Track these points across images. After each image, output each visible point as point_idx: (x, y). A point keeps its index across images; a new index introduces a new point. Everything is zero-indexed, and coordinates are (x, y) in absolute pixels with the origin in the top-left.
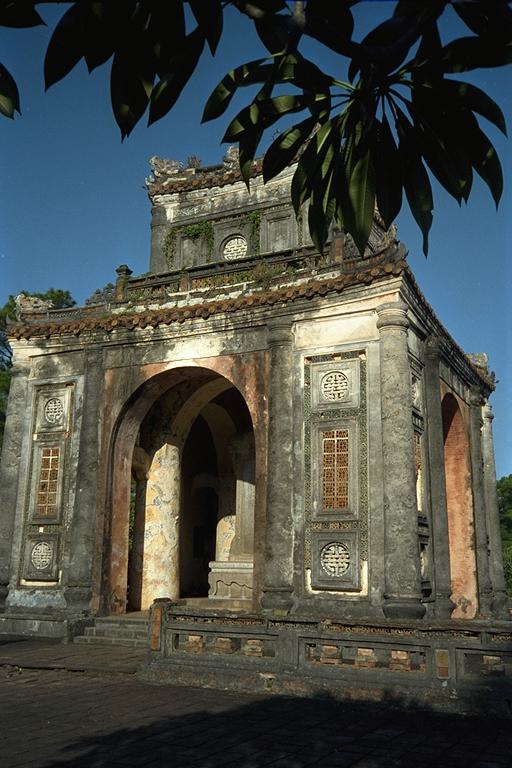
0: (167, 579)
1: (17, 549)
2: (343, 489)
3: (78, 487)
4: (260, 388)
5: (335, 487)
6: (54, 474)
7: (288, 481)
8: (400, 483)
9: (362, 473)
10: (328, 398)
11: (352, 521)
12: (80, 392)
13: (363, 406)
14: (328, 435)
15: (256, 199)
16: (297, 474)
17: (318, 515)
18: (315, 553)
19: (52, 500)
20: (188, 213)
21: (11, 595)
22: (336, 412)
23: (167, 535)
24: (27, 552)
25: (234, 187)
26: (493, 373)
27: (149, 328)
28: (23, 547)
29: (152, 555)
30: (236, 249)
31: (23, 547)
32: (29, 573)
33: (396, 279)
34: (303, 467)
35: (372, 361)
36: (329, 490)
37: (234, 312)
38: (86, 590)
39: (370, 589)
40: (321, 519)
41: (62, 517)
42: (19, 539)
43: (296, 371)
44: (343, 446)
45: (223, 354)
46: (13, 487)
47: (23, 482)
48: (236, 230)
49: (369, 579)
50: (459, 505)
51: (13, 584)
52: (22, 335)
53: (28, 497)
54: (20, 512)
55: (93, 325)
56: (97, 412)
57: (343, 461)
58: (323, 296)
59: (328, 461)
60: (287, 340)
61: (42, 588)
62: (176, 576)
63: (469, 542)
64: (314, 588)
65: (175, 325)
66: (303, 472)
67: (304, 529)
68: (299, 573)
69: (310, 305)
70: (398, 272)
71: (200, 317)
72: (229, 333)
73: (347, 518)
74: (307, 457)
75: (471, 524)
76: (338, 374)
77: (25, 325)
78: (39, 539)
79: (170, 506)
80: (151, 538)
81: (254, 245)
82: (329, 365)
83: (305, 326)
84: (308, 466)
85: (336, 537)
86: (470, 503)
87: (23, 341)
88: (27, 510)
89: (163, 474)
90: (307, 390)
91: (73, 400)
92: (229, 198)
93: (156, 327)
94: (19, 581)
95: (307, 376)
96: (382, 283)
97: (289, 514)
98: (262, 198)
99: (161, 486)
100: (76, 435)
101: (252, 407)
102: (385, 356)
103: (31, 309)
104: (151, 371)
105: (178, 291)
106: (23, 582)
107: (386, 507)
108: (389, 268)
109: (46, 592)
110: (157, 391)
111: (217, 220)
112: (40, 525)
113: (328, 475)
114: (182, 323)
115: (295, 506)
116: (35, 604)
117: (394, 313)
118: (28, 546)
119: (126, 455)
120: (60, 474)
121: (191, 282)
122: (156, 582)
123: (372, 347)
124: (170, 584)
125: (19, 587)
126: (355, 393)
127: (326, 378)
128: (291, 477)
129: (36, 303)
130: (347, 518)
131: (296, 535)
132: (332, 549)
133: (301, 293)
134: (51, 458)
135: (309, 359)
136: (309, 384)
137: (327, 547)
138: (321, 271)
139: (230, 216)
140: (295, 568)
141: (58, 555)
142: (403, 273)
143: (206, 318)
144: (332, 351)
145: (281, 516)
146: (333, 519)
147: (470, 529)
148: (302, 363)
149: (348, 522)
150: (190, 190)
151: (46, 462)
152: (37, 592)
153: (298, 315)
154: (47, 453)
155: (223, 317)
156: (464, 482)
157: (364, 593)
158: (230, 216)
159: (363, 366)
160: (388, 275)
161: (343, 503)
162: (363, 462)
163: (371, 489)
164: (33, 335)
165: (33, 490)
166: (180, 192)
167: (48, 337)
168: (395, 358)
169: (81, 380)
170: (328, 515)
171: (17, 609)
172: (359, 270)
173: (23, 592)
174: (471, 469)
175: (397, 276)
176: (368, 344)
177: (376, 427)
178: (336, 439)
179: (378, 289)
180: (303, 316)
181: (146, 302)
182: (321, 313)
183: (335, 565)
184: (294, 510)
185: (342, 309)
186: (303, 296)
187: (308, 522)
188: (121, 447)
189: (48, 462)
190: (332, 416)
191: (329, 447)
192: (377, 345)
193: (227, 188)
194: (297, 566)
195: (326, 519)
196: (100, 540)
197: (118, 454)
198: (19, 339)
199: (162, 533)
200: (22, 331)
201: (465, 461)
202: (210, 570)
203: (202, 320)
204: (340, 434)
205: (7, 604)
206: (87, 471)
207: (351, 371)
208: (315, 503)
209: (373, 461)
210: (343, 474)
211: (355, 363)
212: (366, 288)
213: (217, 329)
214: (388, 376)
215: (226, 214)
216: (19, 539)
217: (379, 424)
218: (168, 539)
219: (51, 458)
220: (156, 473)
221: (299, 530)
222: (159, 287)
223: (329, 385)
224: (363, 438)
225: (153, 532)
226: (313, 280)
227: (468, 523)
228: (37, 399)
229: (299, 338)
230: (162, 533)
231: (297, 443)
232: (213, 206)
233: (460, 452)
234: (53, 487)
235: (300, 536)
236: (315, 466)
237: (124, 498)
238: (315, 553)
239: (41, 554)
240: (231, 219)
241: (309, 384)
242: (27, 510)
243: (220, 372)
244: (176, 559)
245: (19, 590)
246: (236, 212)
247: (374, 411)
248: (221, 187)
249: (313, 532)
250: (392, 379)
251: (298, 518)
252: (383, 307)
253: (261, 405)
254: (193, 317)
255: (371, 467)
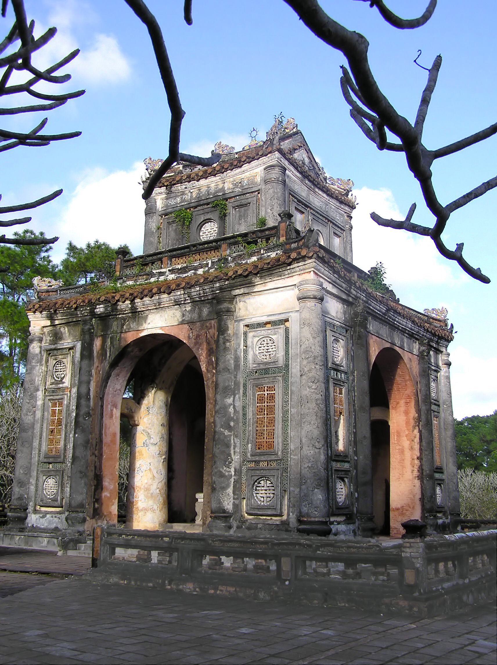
0: (155, 507)
1: (33, 481)
2: (272, 434)
3: (75, 433)
4: (210, 352)
5: (265, 433)
6: (60, 423)
7: (230, 428)
8: (311, 428)
9: (285, 421)
10: (261, 358)
11: (277, 460)
12: (78, 355)
13: (287, 366)
14: (262, 389)
15: (224, 191)
16: (236, 421)
17: (252, 455)
18: (249, 485)
19: (58, 442)
20: (172, 202)
21: (29, 519)
22: (266, 371)
23: (155, 472)
24: (40, 484)
25: (207, 180)
26: (452, 325)
27: (128, 302)
28: (37, 480)
29: (142, 487)
30: (209, 231)
31: (37, 480)
32: (42, 501)
33: (310, 261)
34: (241, 414)
35: (294, 326)
36: (259, 434)
37: (190, 288)
38: (81, 515)
39: (288, 515)
40: (254, 459)
41: (65, 456)
42: (34, 474)
43: (236, 334)
44: (272, 397)
45: (182, 323)
46: (30, 433)
47: (37, 426)
48: (208, 216)
49: (289, 507)
50: (408, 442)
51: (30, 509)
52: (36, 310)
53: (40, 441)
54: (35, 452)
55: (87, 301)
56: (90, 371)
57: (271, 410)
58: (256, 274)
59: (261, 410)
60: (229, 312)
61: (51, 512)
62: (164, 504)
63: (416, 473)
64: (249, 514)
65: (147, 300)
66: (241, 420)
67: (241, 467)
68: (237, 502)
69: (247, 282)
70: (310, 255)
71: (164, 292)
72: (187, 305)
73: (273, 457)
74: (244, 408)
75: (418, 458)
76: (269, 339)
77: (39, 302)
78: (49, 474)
79: (157, 448)
80: (141, 474)
81: (222, 228)
82: (262, 332)
83: (247, 299)
84: (244, 415)
85: (264, 473)
86: (417, 440)
87: (38, 314)
88: (40, 451)
89: (152, 416)
90: (246, 352)
91: (73, 363)
92: (204, 190)
93: (132, 301)
94: (35, 507)
95: (245, 341)
96: (300, 264)
97: (230, 455)
98: (229, 189)
99: (149, 431)
100: (74, 390)
101: (203, 368)
102: (303, 323)
103: (46, 288)
104: (130, 337)
105: (161, 268)
106: (38, 508)
107: (301, 448)
108: (304, 252)
109: (54, 516)
110: (136, 352)
111: (196, 207)
112: (50, 463)
113: (259, 422)
114: (151, 297)
115: (234, 449)
116: (46, 524)
117: (309, 288)
118: (41, 480)
119: (115, 406)
120: (64, 423)
121: (171, 261)
122: (145, 510)
123: (294, 317)
124: (158, 512)
125: (35, 511)
126: (281, 354)
127: (260, 342)
128: (232, 424)
129: (49, 282)
130: (273, 457)
131: (235, 472)
132: (262, 482)
133: (239, 273)
134: (57, 408)
135: (247, 326)
136: (246, 347)
137: (258, 481)
138: (268, 250)
139: (204, 204)
140: (234, 499)
141: (62, 487)
142: (315, 256)
143: (169, 294)
144: (265, 319)
145: (222, 457)
146: (262, 458)
147: (417, 462)
148: (242, 329)
149: (274, 460)
150: (175, 184)
151: (54, 412)
152: (48, 516)
153: (237, 291)
154: (54, 405)
155: (182, 292)
156: (412, 422)
157: (285, 518)
158: (204, 204)
159: (287, 330)
160: (303, 258)
161: (271, 445)
162: (285, 413)
163: (292, 433)
164: (44, 309)
165: (44, 434)
166: (166, 186)
167: (55, 311)
168: (309, 325)
169: (79, 345)
170: (260, 455)
171: (34, 529)
172: (292, 250)
173: (37, 516)
174: (418, 411)
175: (310, 258)
176: (291, 314)
177: (296, 382)
178: (266, 393)
179: (297, 269)
180: (241, 291)
181: (135, 277)
182: (256, 289)
183: (264, 495)
184: (234, 452)
185: (271, 285)
186: (241, 275)
187: (244, 460)
188: (110, 400)
189: (55, 413)
190: (266, 371)
191: (261, 399)
192: (297, 314)
193: (203, 182)
194: (236, 497)
195: (257, 458)
196: (91, 474)
197: (107, 406)
198: (34, 312)
199: (150, 469)
200: (37, 306)
201: (413, 404)
202: (197, 500)
203: (166, 296)
204: (269, 389)
205: (26, 524)
206: (81, 419)
207: (278, 337)
208: (250, 445)
209: (294, 411)
210: (272, 422)
211: (281, 330)
212: (288, 268)
213: (177, 303)
214: (304, 340)
215: (202, 202)
216: (34, 474)
217: (298, 380)
218: (156, 475)
219: (57, 408)
220: (145, 420)
221: (238, 467)
222: (147, 265)
223: (262, 348)
224: (286, 388)
225: (144, 468)
226: (261, 258)
227: (416, 457)
228: (47, 361)
229: (240, 309)
230: (150, 469)
231: (237, 396)
232: (191, 196)
233: (409, 397)
234: (59, 432)
235: (238, 472)
236: (250, 415)
237: (113, 441)
238: (249, 485)
239: (50, 485)
240: (206, 206)
241: (246, 347)
242: (40, 451)
243: (181, 338)
244: (163, 491)
245: (35, 513)
246: (209, 201)
247: (295, 369)
248: (198, 181)
249: (249, 469)
250: (307, 342)
251: (236, 458)
252: (301, 284)
253: (209, 363)
254: (159, 292)
255: (291, 415)
